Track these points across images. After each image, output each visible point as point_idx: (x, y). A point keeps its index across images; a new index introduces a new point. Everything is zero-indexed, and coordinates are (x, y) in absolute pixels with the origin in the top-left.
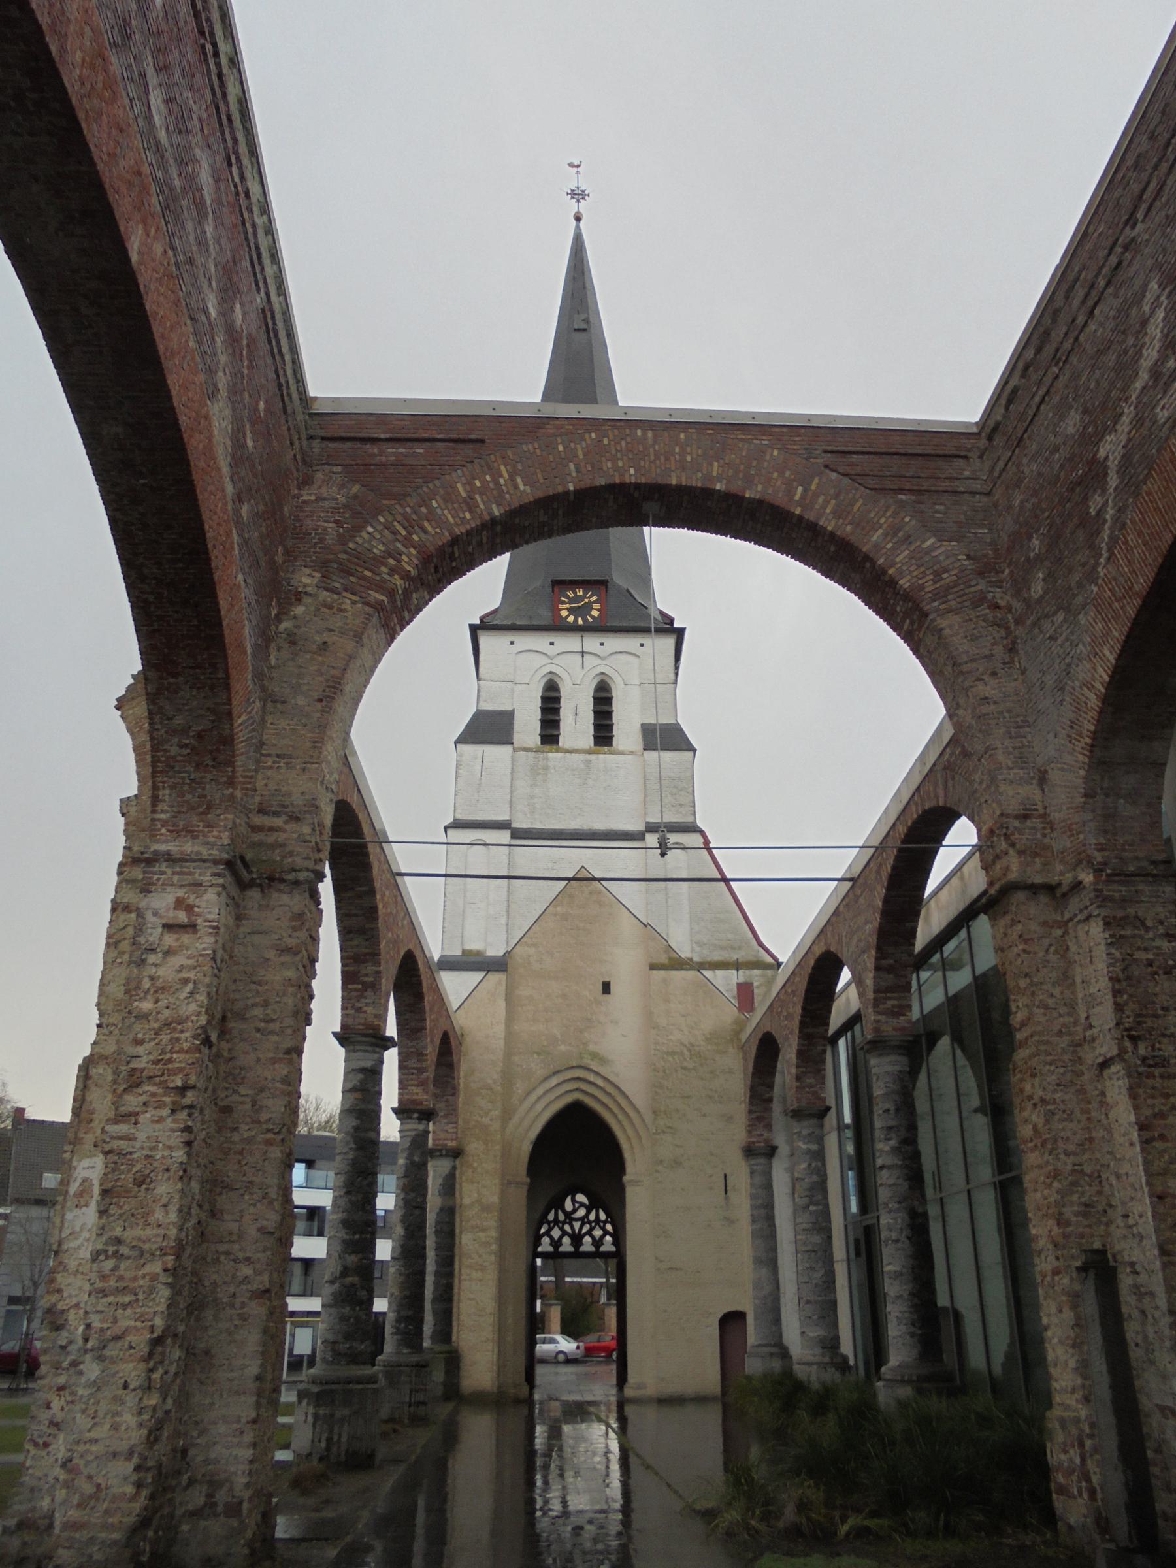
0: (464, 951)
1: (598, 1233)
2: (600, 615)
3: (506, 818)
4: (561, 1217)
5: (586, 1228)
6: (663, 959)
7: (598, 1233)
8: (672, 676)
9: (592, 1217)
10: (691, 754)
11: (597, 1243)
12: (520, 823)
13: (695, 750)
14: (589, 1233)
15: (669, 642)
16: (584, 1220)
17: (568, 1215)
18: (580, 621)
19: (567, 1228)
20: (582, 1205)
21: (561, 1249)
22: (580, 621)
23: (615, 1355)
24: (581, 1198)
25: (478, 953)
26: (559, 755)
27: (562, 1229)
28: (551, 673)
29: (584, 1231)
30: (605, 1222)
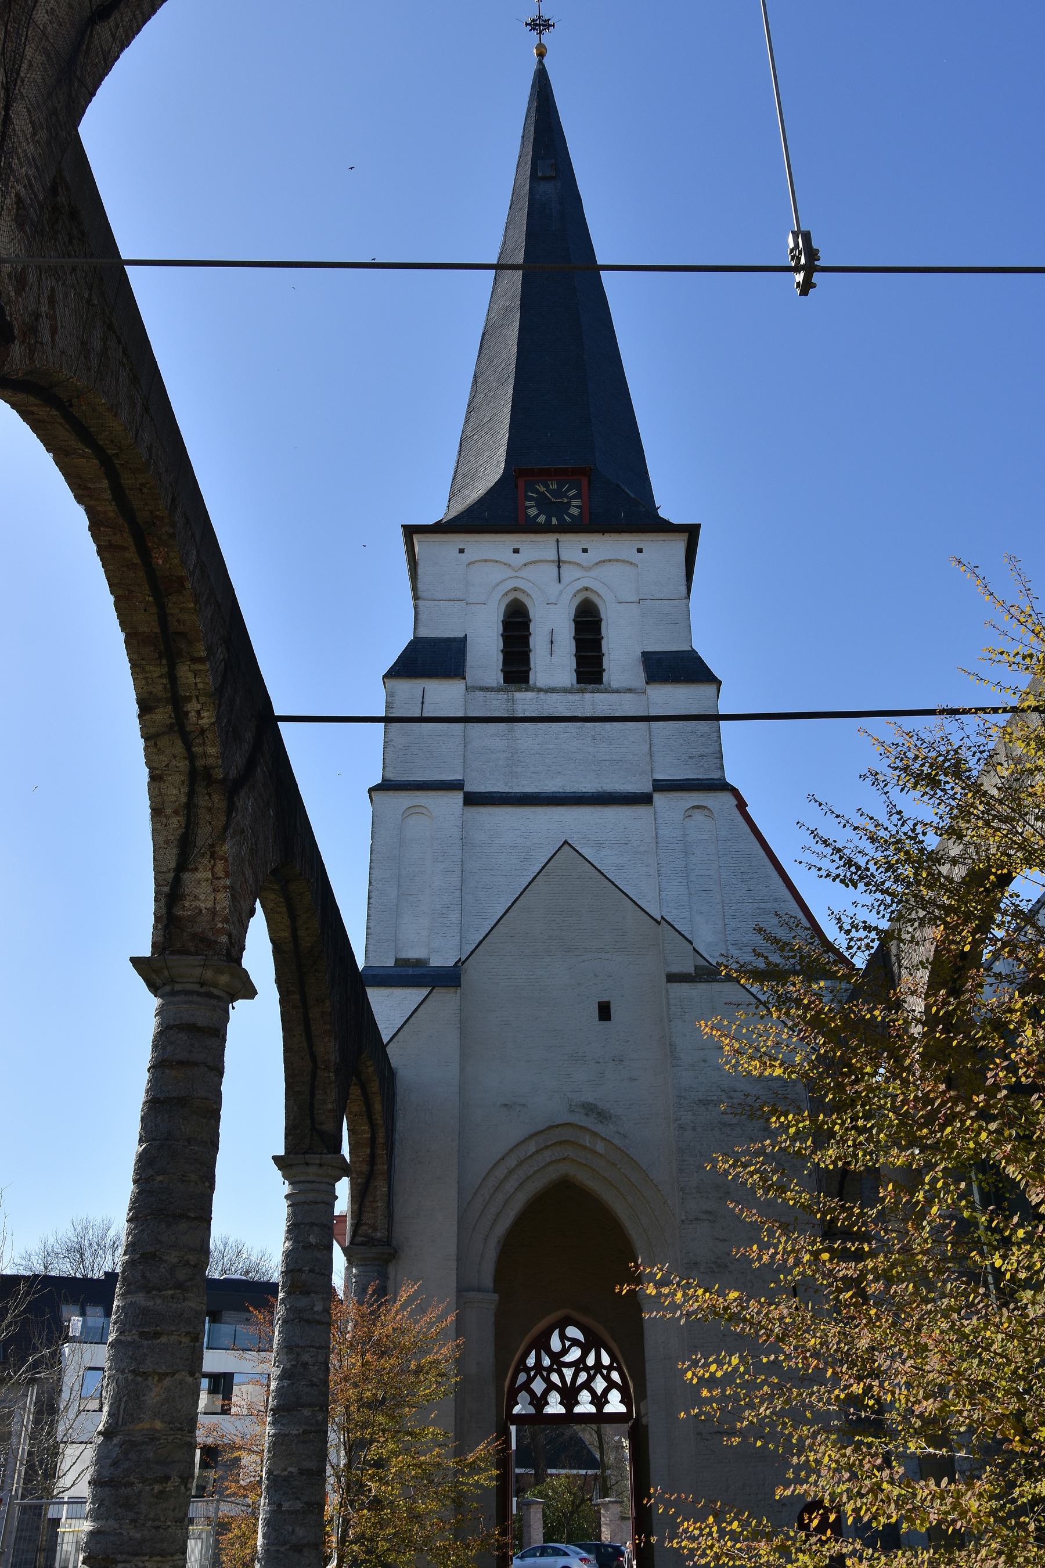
0: (397, 960)
1: (600, 1385)
2: (581, 513)
3: (457, 777)
4: (546, 1362)
5: (583, 1377)
6: (687, 967)
7: (600, 1385)
8: (684, 589)
9: (591, 1361)
10: (713, 688)
11: (599, 1401)
12: (476, 785)
13: (719, 683)
14: (587, 1385)
15: (678, 545)
16: (579, 1365)
17: (556, 1357)
18: (554, 521)
19: (555, 1378)
20: (575, 1342)
21: (608, 1409)
22: (554, 521)
23: (176, 728)
24: (573, 1332)
25: (419, 963)
26: (530, 695)
27: (547, 1380)
28: (515, 589)
29: (579, 1381)
30: (610, 1368)
